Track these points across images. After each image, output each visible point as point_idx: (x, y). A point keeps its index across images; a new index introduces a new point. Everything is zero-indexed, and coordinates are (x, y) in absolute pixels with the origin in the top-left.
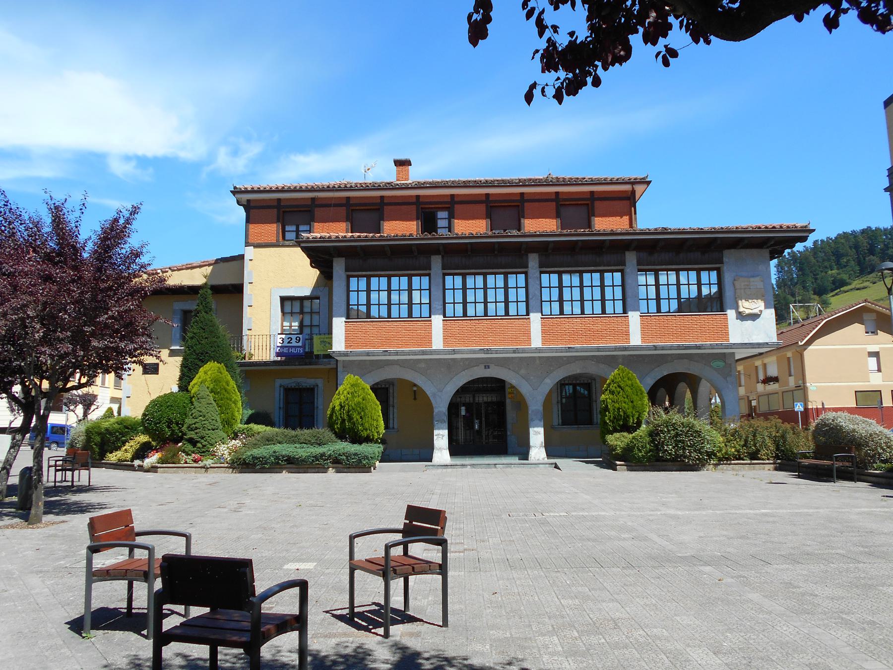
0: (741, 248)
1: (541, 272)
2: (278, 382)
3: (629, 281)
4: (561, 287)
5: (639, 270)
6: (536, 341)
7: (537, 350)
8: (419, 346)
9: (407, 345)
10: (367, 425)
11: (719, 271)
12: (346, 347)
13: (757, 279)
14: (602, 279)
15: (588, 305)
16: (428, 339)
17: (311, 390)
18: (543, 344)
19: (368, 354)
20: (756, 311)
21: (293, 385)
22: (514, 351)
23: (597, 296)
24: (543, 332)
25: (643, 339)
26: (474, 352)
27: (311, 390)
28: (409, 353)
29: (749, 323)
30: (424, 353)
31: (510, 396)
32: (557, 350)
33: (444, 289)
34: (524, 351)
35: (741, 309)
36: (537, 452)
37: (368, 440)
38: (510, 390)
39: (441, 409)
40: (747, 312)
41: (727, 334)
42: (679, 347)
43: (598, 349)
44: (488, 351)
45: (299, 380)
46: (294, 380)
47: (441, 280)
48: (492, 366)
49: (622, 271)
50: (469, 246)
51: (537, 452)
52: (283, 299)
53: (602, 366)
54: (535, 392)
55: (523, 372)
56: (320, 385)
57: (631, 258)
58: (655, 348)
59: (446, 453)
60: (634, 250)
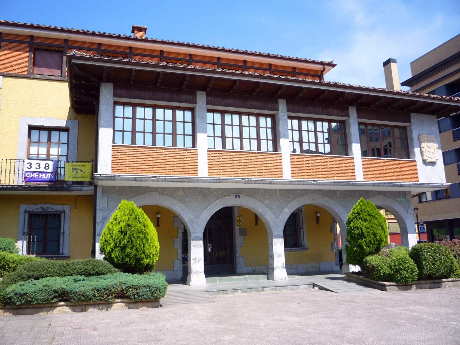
0: (422, 113)
1: (116, 103)
2: (23, 208)
3: (198, 121)
4: (154, 120)
5: (209, 111)
6: (287, 175)
7: (290, 183)
8: (188, 173)
9: (174, 172)
10: (148, 253)
11: (273, 118)
12: (113, 171)
13: (433, 136)
14: (134, 113)
15: (139, 137)
16: (195, 168)
17: (57, 216)
18: (209, 175)
19: (136, 179)
20: (434, 160)
21: (39, 211)
22: (270, 183)
23: (237, 134)
24: (293, 166)
25: (365, 177)
26: (237, 182)
27: (57, 216)
28: (176, 181)
29: (430, 168)
30: (191, 181)
31: (238, 223)
32: (304, 184)
33: (114, 117)
34: (278, 183)
35: (425, 158)
36: (280, 273)
37: (148, 268)
38: (238, 219)
39: (197, 235)
40: (430, 160)
41: (417, 176)
42: (389, 185)
43: (335, 184)
44: (248, 182)
45: (45, 206)
46: (40, 206)
47: (112, 108)
48: (241, 195)
49: (192, 110)
50: (326, 92)
51: (280, 273)
52: (31, 128)
53: (326, 199)
54: (276, 219)
55: (267, 201)
56: (67, 211)
57: (201, 98)
58: (374, 185)
59: (284, 272)
60: (355, 106)
